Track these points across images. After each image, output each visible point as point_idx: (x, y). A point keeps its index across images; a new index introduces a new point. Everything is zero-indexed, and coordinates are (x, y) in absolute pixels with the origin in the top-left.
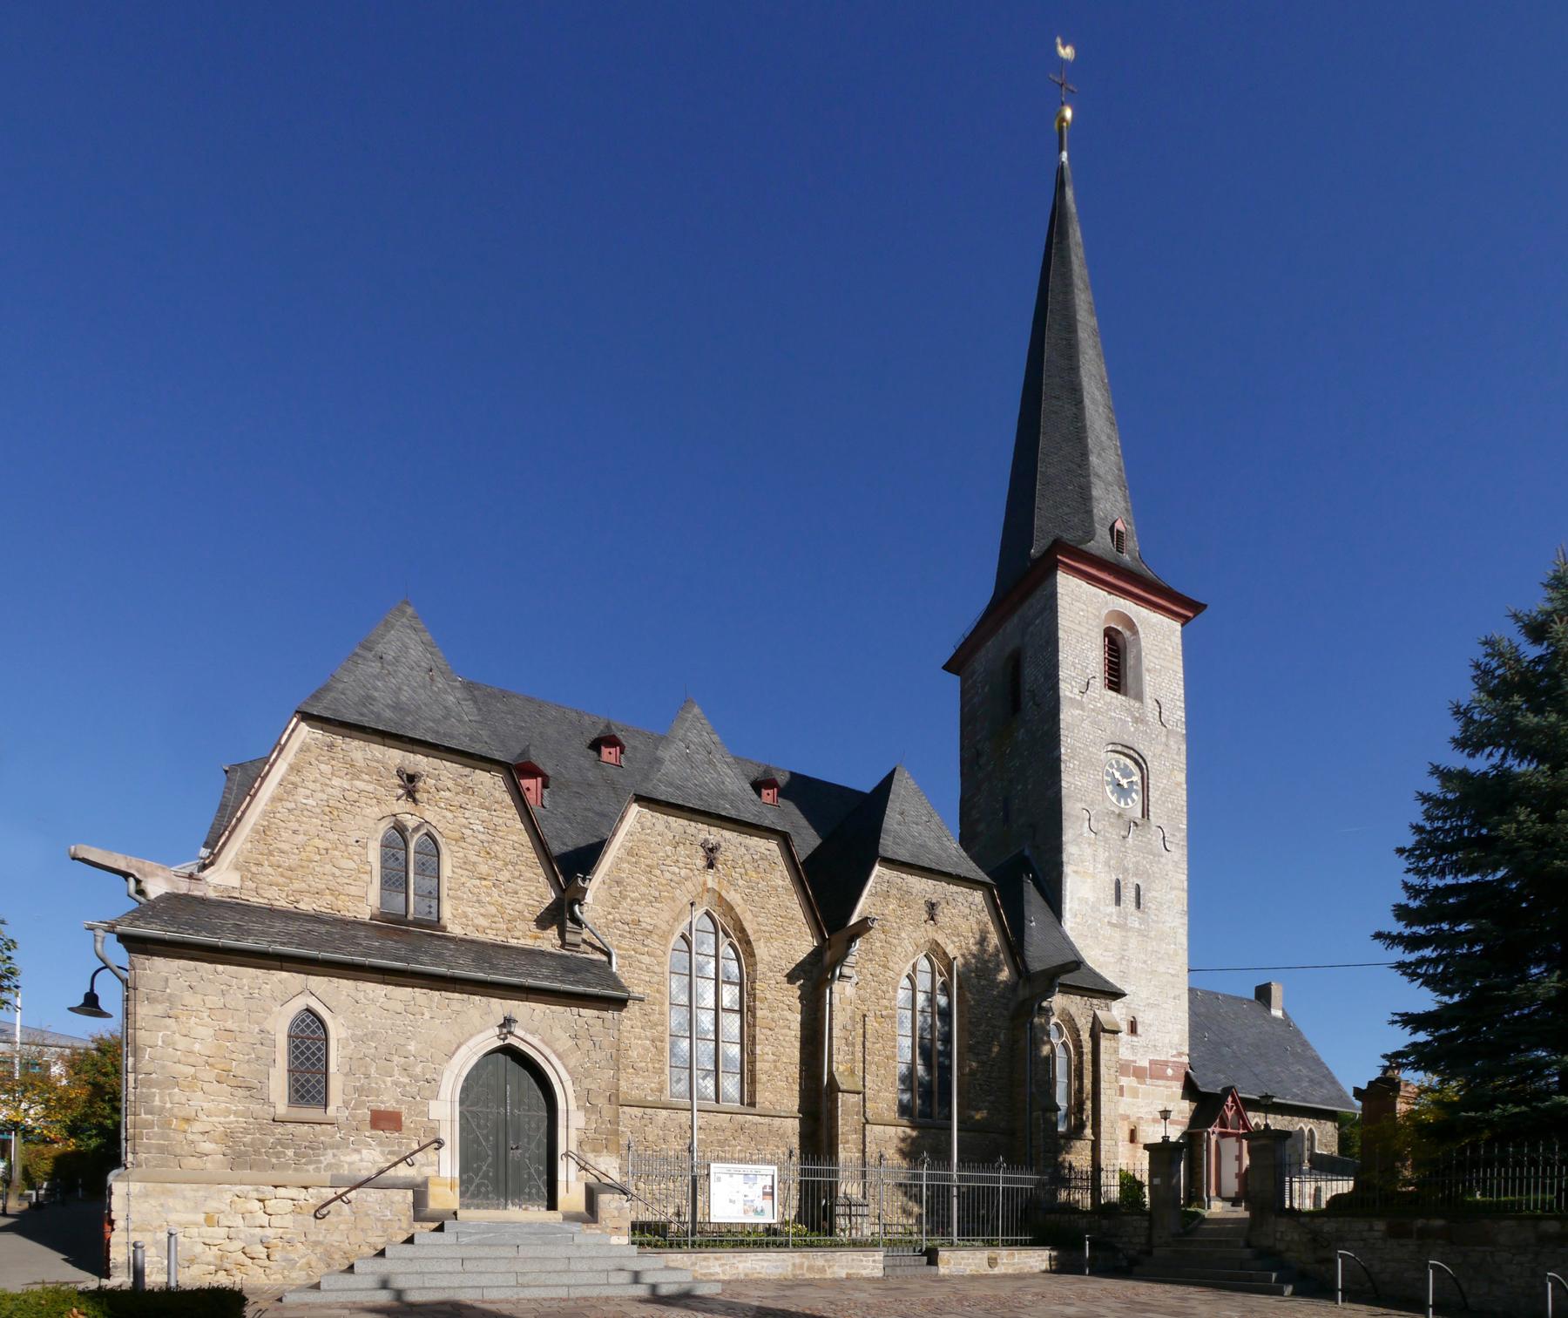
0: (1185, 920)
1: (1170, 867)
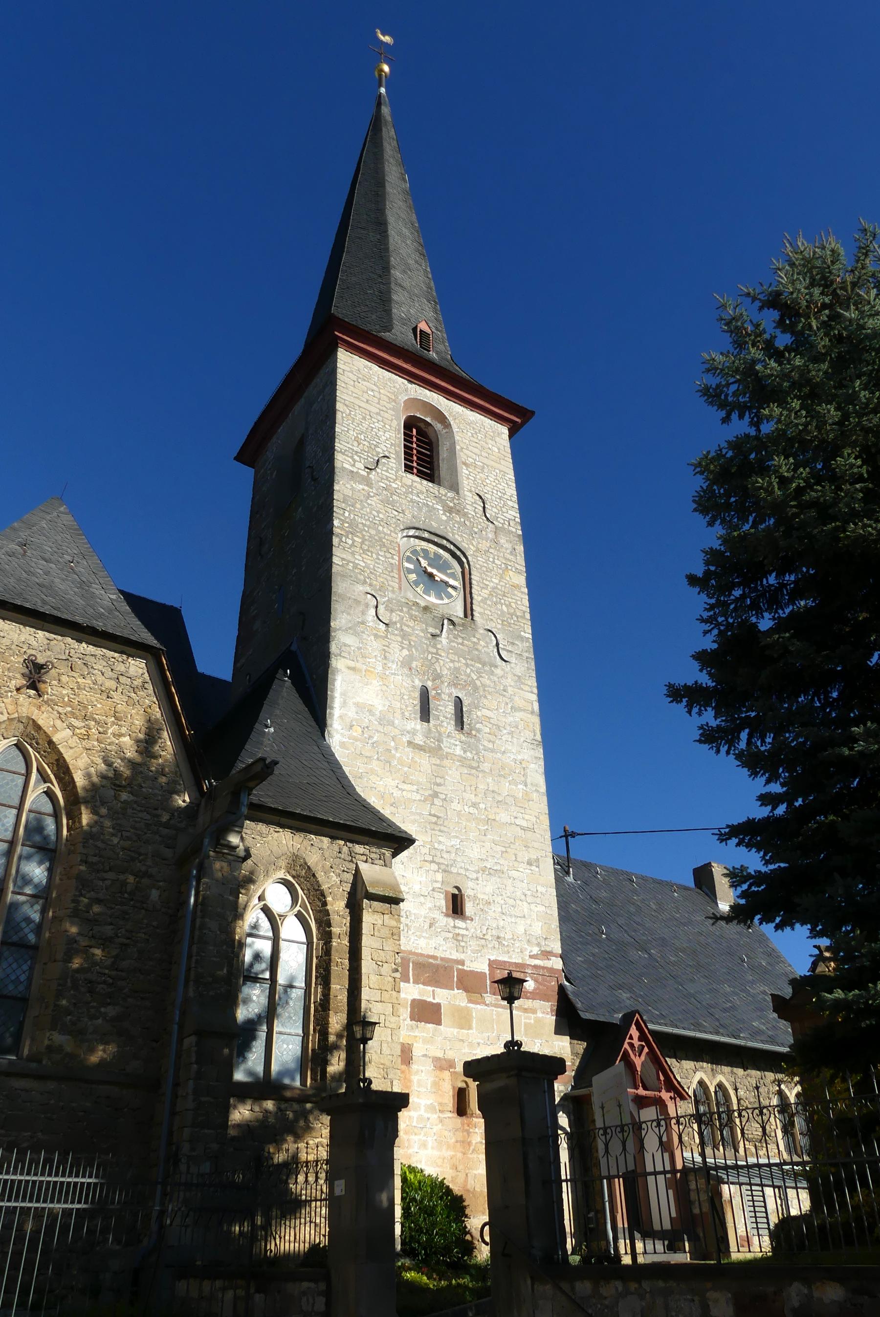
0: (540, 752)
1: (509, 681)
